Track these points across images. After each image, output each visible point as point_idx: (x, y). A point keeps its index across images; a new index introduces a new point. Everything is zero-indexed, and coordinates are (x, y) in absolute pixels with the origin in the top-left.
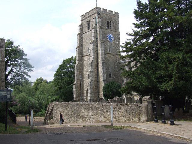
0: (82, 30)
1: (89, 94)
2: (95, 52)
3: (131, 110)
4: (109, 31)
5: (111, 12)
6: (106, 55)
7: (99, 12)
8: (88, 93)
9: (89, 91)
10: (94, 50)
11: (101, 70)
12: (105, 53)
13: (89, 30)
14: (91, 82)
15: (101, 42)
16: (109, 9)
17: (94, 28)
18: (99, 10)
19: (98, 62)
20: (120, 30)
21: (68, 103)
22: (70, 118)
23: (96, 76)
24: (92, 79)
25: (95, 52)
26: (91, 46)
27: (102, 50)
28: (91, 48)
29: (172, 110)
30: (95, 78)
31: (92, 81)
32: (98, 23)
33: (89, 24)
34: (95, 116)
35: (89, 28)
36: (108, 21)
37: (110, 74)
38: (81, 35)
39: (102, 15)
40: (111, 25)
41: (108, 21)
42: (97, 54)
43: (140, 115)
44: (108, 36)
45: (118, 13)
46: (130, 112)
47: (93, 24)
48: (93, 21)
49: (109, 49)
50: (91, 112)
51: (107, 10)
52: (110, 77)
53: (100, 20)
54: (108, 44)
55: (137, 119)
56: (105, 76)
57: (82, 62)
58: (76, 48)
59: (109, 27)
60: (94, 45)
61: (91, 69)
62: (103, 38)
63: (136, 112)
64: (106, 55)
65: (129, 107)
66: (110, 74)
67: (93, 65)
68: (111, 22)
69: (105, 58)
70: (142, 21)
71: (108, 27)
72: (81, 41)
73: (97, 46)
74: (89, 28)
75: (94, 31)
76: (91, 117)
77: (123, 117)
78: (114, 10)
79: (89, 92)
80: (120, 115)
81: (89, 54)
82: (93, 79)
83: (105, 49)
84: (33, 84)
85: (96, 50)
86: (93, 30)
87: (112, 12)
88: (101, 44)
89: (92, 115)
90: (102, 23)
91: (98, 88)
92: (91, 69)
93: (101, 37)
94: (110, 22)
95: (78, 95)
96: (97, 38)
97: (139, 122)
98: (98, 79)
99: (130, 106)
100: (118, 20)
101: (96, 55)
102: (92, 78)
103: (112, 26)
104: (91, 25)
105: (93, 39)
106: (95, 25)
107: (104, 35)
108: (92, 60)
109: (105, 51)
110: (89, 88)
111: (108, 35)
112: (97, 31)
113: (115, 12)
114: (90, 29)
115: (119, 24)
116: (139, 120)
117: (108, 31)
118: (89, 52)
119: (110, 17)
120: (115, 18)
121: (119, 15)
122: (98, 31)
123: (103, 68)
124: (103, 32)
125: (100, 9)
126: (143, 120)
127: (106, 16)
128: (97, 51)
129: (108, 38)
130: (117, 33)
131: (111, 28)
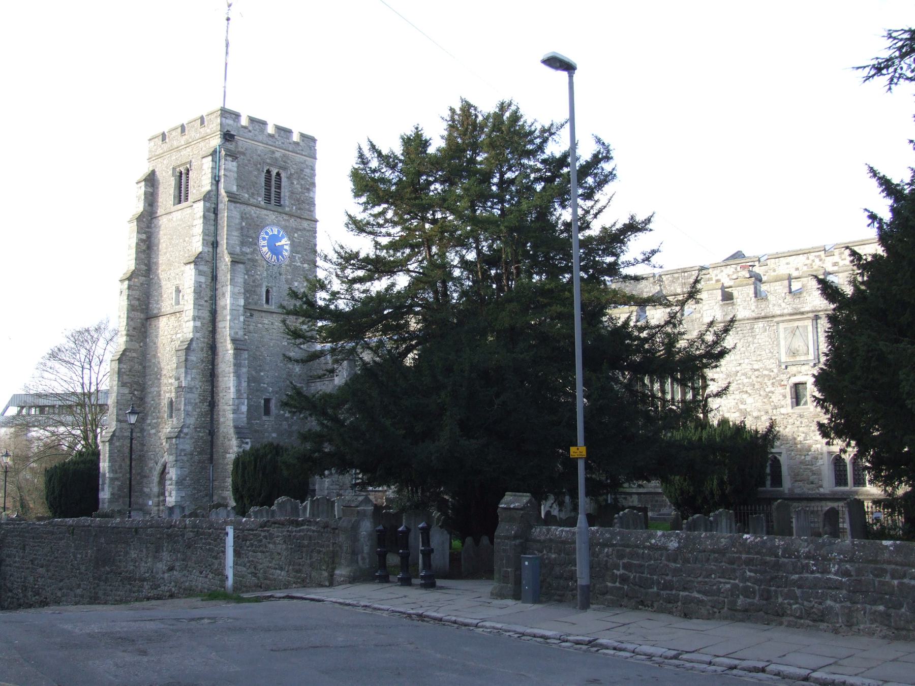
0: (151, 199)
1: (170, 487)
2: (203, 302)
3: (306, 542)
4: (272, 216)
5: (284, 132)
6: (252, 315)
7: (234, 136)
8: (168, 482)
9: (173, 474)
10: (198, 292)
11: (228, 384)
12: (246, 308)
13: (184, 204)
14: (181, 431)
15: (234, 262)
16: (273, 121)
17: (207, 198)
18: (230, 122)
19: (213, 348)
20: (319, 213)
21: (70, 521)
22: (79, 586)
23: (205, 407)
24: (188, 422)
25: (203, 302)
26: (188, 278)
27: (233, 295)
28: (186, 286)
29: (379, 531)
30: (201, 415)
31: (186, 430)
32: (222, 180)
33: (184, 176)
34: (181, 570)
35: (181, 195)
36: (268, 172)
37: (267, 401)
38: (147, 222)
39: (243, 143)
40: (279, 187)
41: (268, 172)
42: (214, 313)
43: (333, 561)
44: (263, 235)
45: (313, 140)
46: (304, 549)
47: (201, 182)
48: (201, 168)
49: (268, 292)
50: (165, 555)
51: (264, 123)
52: (267, 412)
53: (232, 165)
54: (261, 272)
55: (325, 574)
56: (244, 408)
57: (145, 344)
58: (122, 281)
59: (273, 198)
60: (200, 273)
61: (182, 379)
62: (243, 244)
63: (324, 550)
64: (252, 315)
65: (300, 531)
66: (267, 401)
67: (193, 358)
68: (283, 175)
69: (247, 332)
70: (378, 209)
71: (268, 198)
72: (147, 247)
73: (214, 278)
74: (181, 195)
75: (206, 210)
76: (166, 575)
77: (281, 569)
78: (297, 129)
79: (168, 476)
80: (270, 562)
81: (177, 308)
82: (191, 421)
83: (249, 291)
84: (457, 543)
85: (209, 293)
86: (199, 208)
87: (289, 132)
88: (233, 271)
89: (171, 569)
90: (242, 179)
91: (211, 459)
92: (182, 379)
93: (235, 240)
94: (278, 174)
95: (120, 488)
96: (215, 245)
97: (331, 585)
98: (212, 419)
99: (305, 527)
100: (313, 169)
101: (206, 314)
102: (188, 414)
103: (285, 192)
104: (191, 183)
105: (197, 246)
106: (208, 188)
107: (248, 233)
108: (191, 336)
109: (246, 299)
110: (168, 458)
111: (267, 233)
112: (216, 212)
113: (303, 136)
114: (187, 200)
115: (313, 184)
116: (332, 575)
117: (265, 212)
118: (178, 303)
119: (278, 155)
120: (299, 158)
121: (319, 146)
122: (224, 215)
123: (238, 376)
124: (242, 218)
125: (237, 116)
126: (341, 576)
127: (261, 147)
128: (214, 299)
129: (265, 249)
130: (305, 224)
131: (278, 203)
